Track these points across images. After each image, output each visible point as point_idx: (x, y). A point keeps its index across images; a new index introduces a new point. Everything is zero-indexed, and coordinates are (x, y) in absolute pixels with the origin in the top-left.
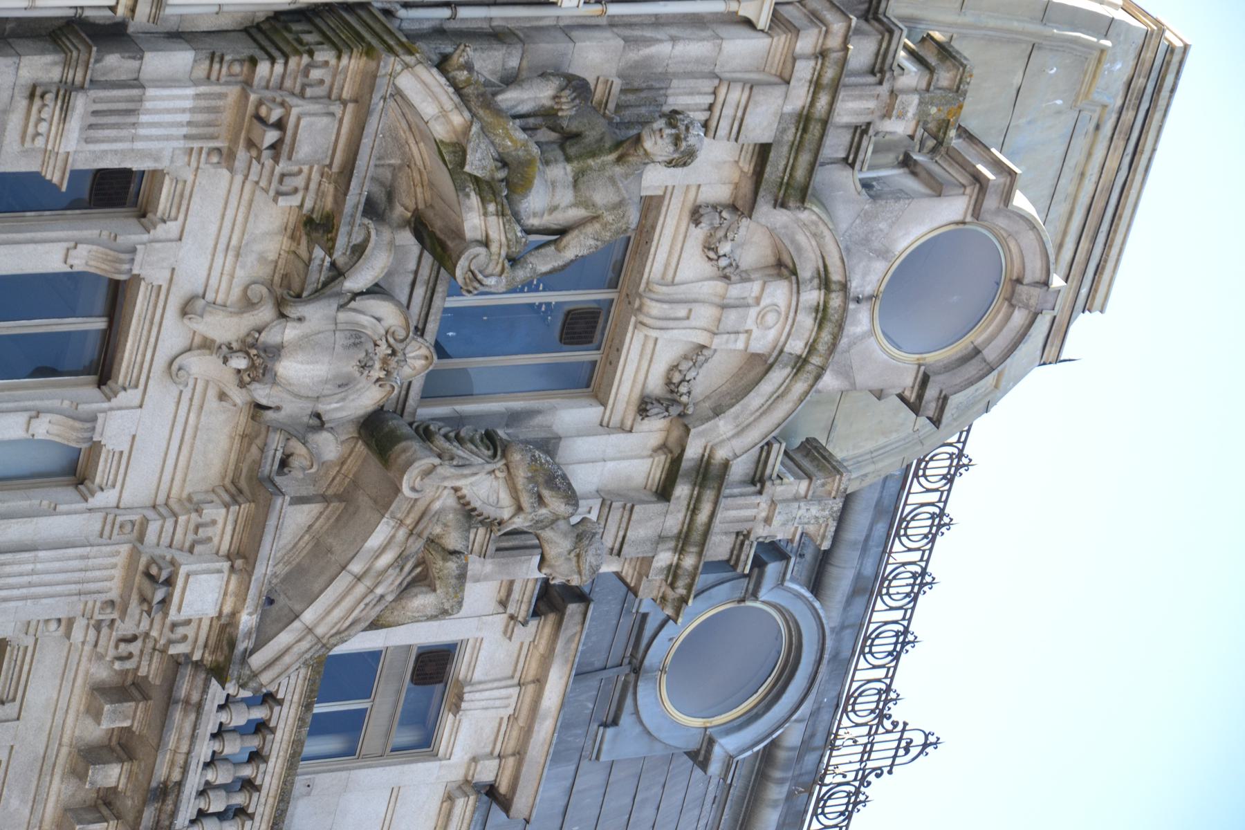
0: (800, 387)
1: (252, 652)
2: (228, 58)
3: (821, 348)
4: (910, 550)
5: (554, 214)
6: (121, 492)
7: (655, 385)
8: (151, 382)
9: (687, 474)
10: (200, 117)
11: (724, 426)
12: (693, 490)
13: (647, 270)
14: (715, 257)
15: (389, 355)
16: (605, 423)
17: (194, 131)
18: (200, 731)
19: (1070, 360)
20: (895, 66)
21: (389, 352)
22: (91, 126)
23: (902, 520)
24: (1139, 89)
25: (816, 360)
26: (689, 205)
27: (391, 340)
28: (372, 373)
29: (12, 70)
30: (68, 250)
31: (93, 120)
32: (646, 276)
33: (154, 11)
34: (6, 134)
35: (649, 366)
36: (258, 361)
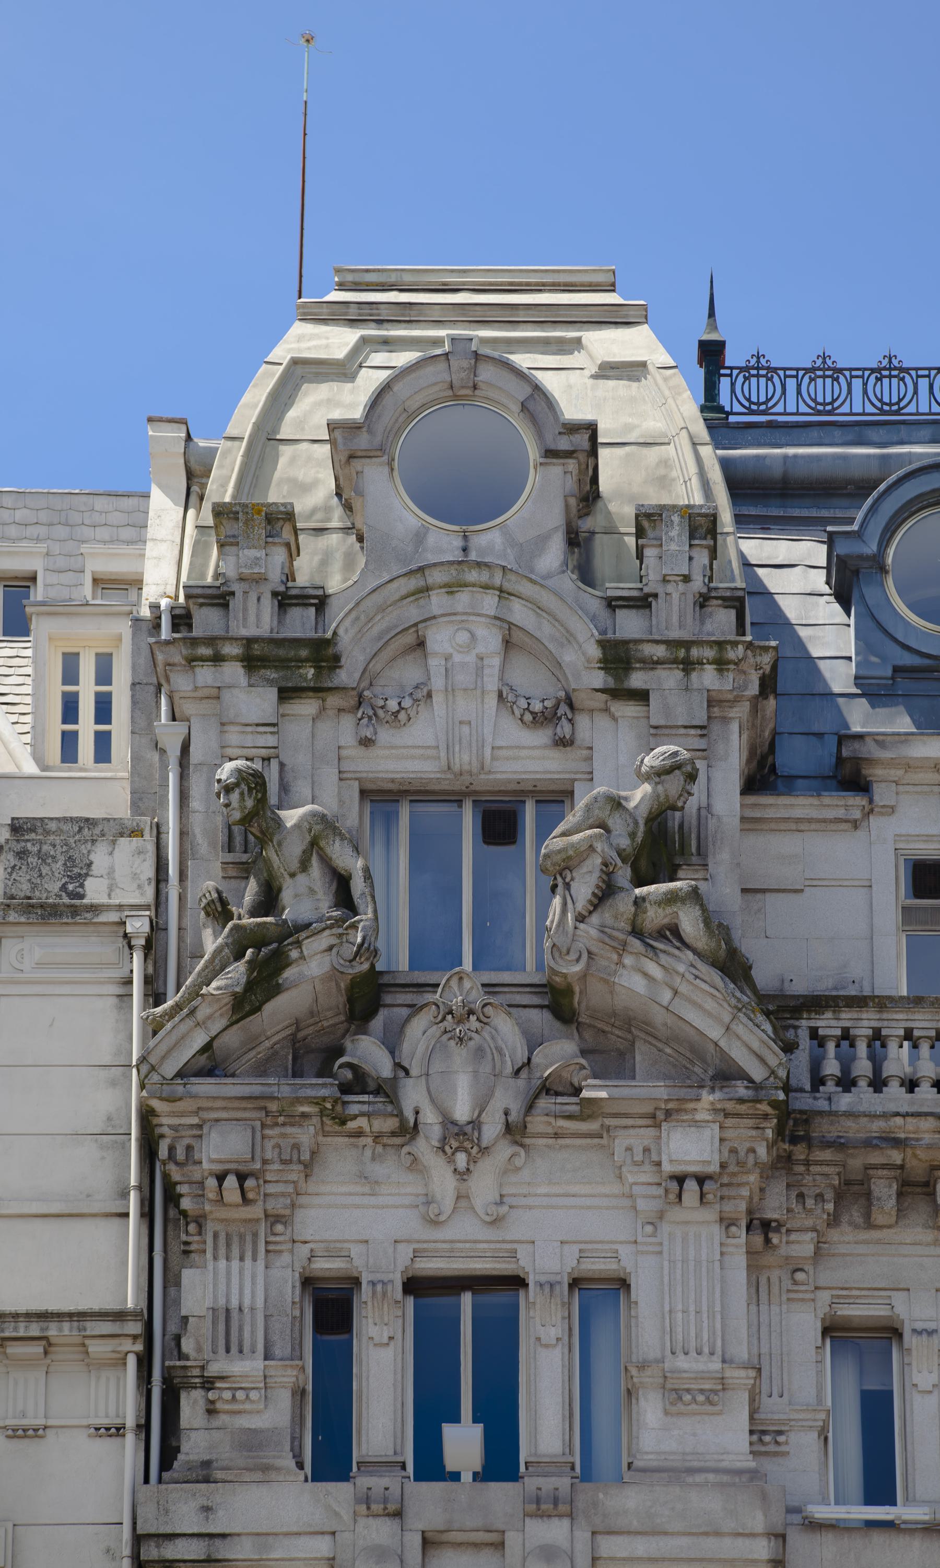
0: (525, 588)
1: (751, 1081)
2: (184, 1237)
3: (484, 577)
4: (916, 392)
5: (316, 889)
6: (621, 1243)
7: (542, 737)
8: (508, 1238)
9: (617, 678)
10: (236, 1252)
11: (569, 657)
12: (637, 668)
13: (432, 776)
14: (403, 712)
15: (453, 1017)
16: (589, 777)
17: (248, 1255)
18: (879, 1110)
19: (712, 282)
20: (217, 583)
21: (449, 1017)
22: (241, 1351)
23: (883, 412)
24: (359, 309)
25: (497, 580)
26: (361, 751)
27: (440, 1017)
28: (474, 1029)
29: (193, 1435)
30: (375, 1345)
31: (234, 1349)
32: (439, 776)
33: (130, 1318)
34: (253, 1427)
35: (524, 748)
36: (455, 1144)
